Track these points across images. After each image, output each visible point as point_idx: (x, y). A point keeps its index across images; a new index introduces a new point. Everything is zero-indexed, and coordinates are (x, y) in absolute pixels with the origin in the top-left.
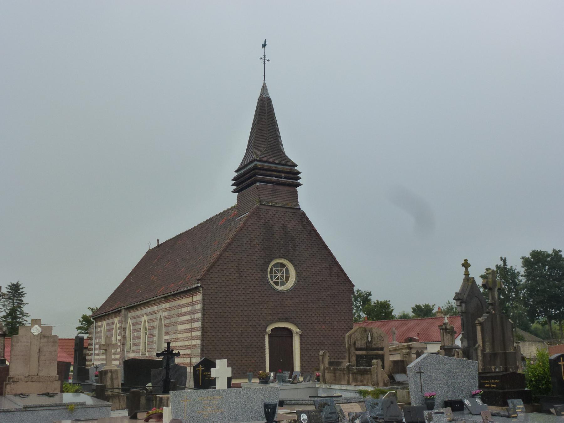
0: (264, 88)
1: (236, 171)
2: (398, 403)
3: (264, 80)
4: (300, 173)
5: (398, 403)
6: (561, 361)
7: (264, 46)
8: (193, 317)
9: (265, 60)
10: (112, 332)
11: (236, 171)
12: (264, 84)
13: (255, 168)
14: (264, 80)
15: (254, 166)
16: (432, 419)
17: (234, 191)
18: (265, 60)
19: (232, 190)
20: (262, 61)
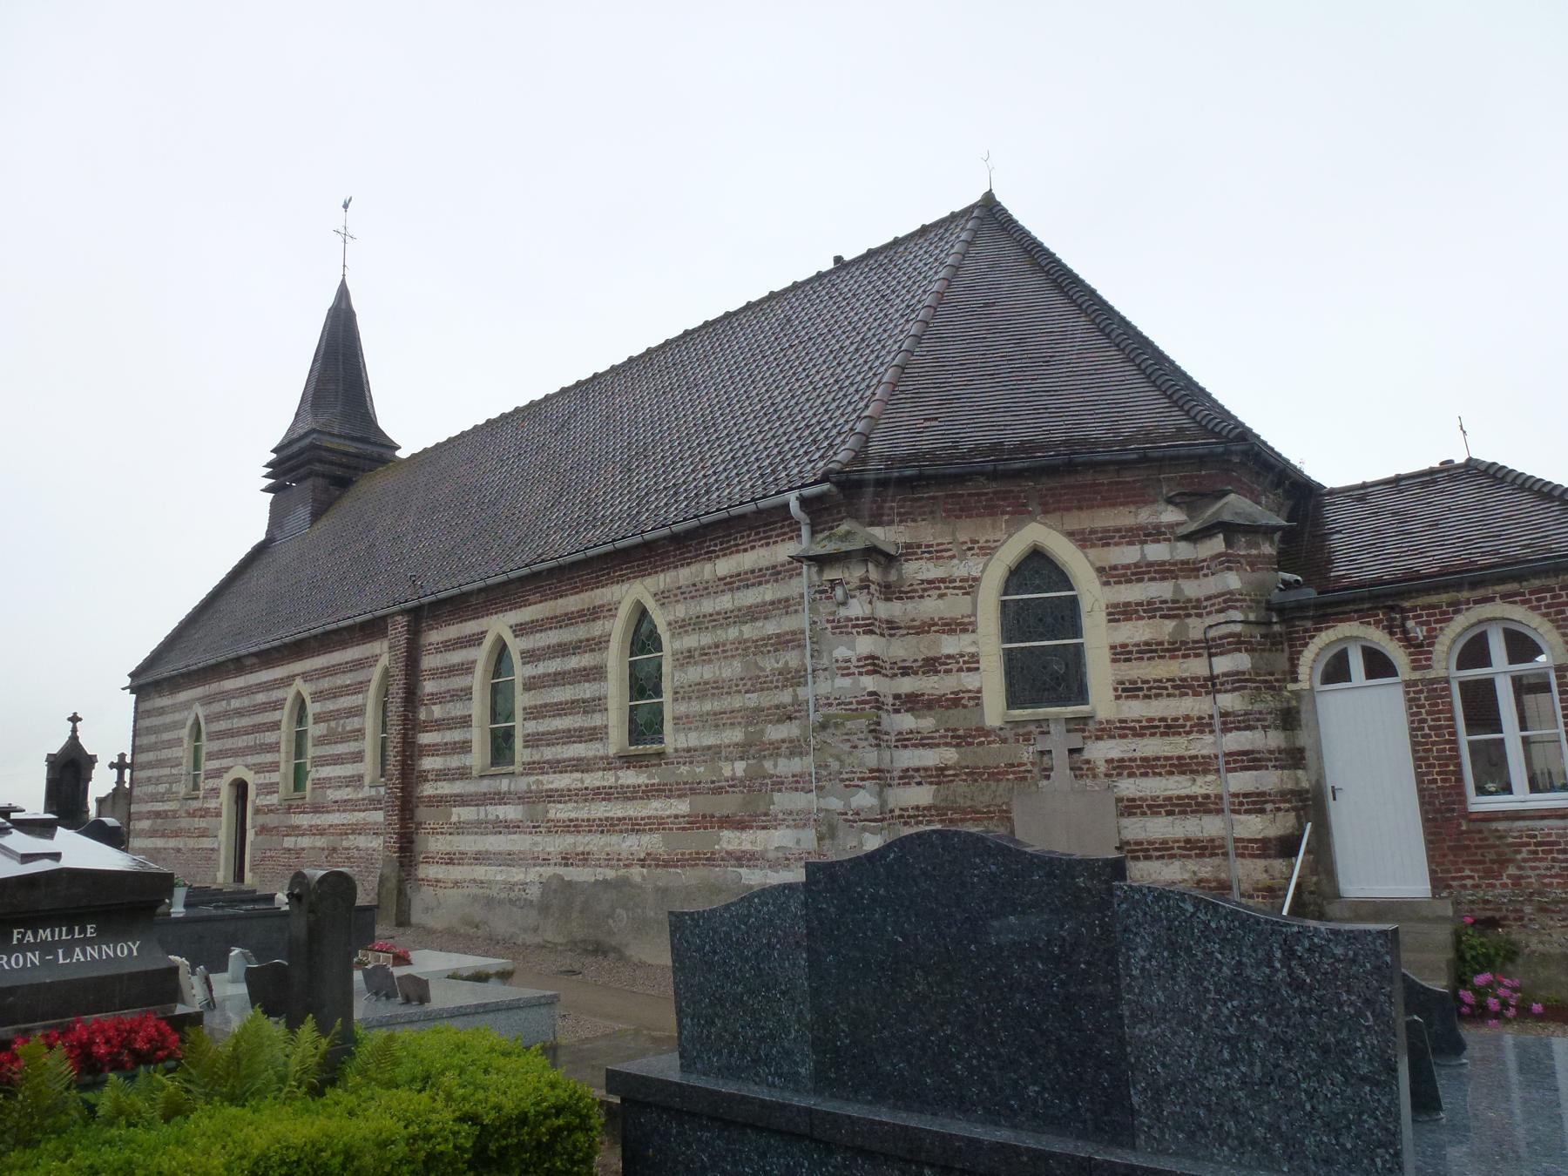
0: (343, 293)
1: (274, 451)
2: (1285, 912)
3: (344, 275)
4: (399, 448)
5: (1285, 912)
6: (1010, 641)
7: (346, 206)
8: (482, 816)
9: (345, 236)
10: (1280, 900)
11: (274, 451)
12: (343, 282)
13: (313, 447)
14: (344, 275)
15: (311, 443)
16: (159, 688)
17: (266, 490)
18: (345, 236)
19: (263, 487)
20: (340, 238)
